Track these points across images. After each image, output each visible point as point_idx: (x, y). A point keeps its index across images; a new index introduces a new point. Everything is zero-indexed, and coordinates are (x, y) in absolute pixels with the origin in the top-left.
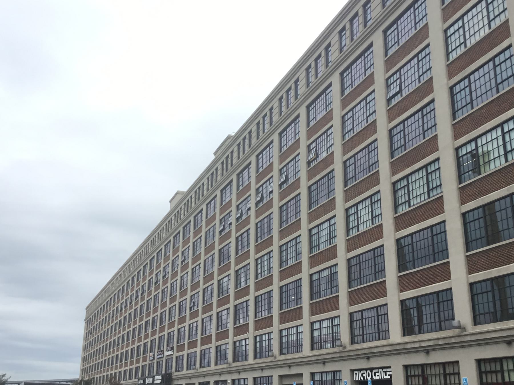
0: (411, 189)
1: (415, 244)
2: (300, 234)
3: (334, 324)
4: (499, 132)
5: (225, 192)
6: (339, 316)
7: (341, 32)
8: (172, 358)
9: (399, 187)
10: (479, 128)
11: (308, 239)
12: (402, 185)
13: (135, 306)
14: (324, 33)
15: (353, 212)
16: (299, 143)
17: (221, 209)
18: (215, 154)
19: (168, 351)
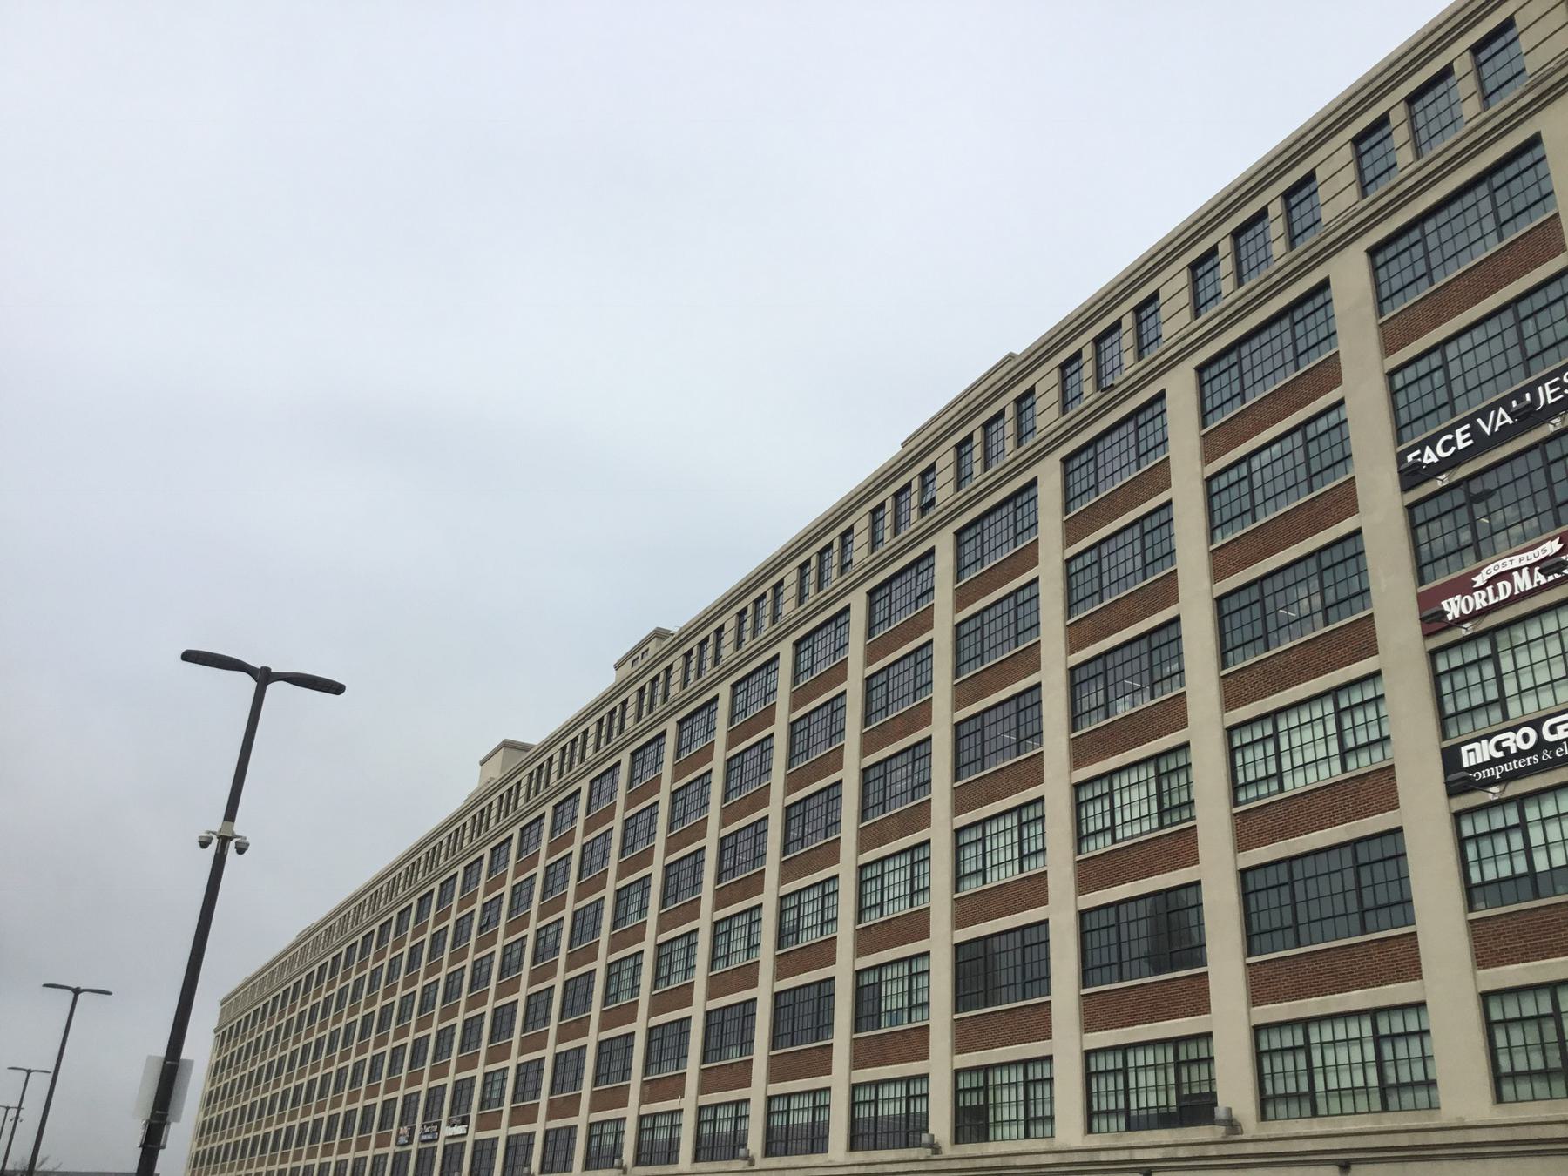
0: (988, 849)
1: (1124, 928)
2: (835, 874)
3: (817, 1104)
4: (1145, 648)
5: (562, 811)
6: (829, 1089)
7: (874, 512)
8: (464, 1144)
9: (967, 841)
10: (1282, 693)
11: (1072, 815)
12: (973, 838)
13: (334, 1023)
14: (1100, 300)
15: (874, 875)
16: (846, 670)
17: (628, 796)
18: (904, 445)
19: (453, 1126)
